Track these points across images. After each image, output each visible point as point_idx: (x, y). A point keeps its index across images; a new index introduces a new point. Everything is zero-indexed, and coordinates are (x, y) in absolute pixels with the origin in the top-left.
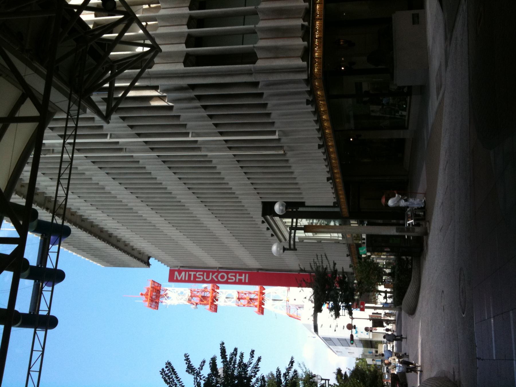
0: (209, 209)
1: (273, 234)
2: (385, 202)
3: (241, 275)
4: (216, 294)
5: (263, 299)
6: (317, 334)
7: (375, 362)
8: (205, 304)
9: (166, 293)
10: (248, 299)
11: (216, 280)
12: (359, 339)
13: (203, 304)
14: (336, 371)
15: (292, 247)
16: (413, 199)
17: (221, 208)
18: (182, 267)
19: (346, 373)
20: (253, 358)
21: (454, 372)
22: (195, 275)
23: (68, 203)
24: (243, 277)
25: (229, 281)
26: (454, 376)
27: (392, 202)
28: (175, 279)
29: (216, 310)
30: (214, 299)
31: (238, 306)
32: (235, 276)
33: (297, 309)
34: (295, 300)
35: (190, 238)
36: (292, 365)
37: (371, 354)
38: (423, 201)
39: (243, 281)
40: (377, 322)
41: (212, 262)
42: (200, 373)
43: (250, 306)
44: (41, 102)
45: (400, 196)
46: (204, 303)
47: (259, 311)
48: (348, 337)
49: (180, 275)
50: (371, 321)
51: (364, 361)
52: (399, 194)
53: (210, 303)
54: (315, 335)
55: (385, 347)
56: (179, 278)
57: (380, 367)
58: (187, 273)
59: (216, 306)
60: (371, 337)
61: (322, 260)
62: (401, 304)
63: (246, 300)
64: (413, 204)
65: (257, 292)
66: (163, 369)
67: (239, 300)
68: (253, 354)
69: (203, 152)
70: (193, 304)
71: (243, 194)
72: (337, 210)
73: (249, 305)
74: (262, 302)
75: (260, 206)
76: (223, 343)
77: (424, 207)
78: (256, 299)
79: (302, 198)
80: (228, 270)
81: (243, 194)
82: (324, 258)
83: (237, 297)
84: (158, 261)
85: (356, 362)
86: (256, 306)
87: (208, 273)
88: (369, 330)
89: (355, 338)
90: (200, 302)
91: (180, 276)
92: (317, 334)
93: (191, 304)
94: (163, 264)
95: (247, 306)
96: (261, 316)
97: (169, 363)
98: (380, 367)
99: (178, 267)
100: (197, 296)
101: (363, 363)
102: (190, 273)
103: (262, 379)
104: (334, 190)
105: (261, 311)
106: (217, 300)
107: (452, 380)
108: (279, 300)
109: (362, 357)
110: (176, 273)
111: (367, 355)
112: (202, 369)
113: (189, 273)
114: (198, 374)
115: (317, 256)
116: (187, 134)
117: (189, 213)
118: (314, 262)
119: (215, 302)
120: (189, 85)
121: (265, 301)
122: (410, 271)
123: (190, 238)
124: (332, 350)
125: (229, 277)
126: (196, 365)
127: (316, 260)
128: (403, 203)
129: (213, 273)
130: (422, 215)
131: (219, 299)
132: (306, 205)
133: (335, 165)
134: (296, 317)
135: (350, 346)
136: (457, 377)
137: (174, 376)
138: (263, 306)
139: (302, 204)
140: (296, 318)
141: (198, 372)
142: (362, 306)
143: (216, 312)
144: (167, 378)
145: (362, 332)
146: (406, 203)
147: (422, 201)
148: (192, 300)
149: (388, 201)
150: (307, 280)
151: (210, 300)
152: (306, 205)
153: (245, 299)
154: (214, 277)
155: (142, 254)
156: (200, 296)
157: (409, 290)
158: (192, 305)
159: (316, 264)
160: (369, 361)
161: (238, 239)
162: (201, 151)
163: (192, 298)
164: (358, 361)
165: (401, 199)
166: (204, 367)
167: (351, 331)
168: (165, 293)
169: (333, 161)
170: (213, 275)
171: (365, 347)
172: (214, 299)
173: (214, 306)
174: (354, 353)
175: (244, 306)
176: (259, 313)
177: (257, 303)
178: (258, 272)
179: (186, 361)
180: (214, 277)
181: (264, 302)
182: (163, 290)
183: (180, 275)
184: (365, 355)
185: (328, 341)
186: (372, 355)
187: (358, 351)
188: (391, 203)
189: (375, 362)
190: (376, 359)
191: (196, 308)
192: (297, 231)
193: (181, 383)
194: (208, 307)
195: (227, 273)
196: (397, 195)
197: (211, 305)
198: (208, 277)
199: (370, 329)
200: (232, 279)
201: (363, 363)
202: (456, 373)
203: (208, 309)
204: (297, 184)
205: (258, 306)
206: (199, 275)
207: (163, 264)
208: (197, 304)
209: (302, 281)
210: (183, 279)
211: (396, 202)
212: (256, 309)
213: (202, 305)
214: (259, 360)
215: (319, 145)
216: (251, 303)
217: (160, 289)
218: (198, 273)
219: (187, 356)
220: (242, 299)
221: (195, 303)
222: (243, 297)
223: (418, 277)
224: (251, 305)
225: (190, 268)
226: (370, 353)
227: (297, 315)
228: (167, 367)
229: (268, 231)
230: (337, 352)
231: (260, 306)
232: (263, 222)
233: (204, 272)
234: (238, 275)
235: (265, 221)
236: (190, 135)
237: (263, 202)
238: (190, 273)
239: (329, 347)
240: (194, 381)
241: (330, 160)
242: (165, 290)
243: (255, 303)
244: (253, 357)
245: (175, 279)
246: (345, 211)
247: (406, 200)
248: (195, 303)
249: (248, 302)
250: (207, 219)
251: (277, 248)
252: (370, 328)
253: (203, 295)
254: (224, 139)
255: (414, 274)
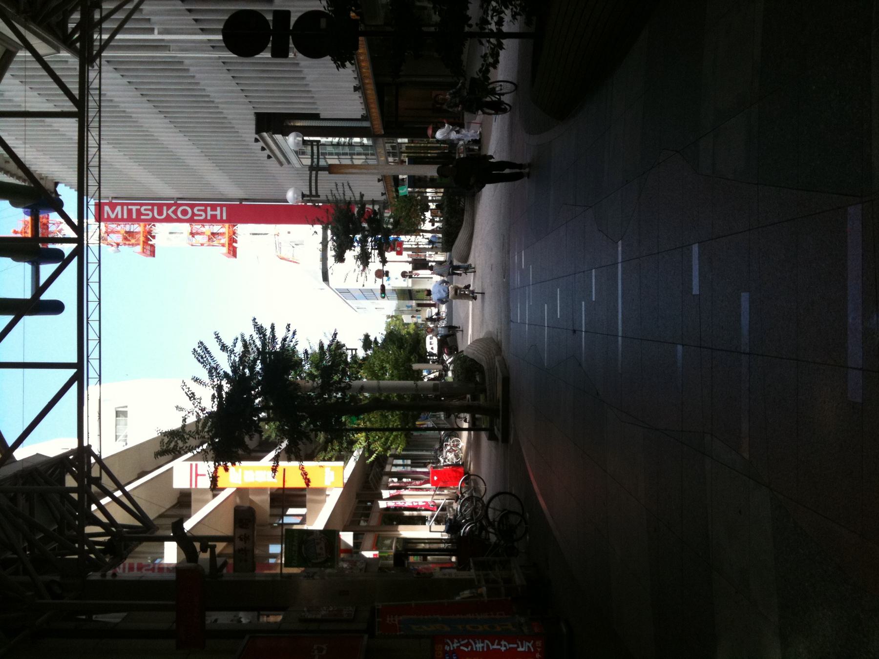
0: (136, 89)
1: (270, 154)
2: (432, 134)
3: (214, 207)
4: (151, 227)
5: (234, 233)
6: (328, 285)
7: (415, 320)
8: (133, 245)
9: (59, 228)
10: (209, 234)
11: (174, 216)
12: (391, 288)
13: (129, 245)
14: (362, 337)
15: (314, 193)
16: (467, 130)
17: (161, 93)
18: (116, 198)
19: (376, 338)
20: (289, 332)
21: (497, 332)
22: (138, 211)
23: (102, 194)
24: (218, 212)
25: (196, 218)
26: (497, 336)
27: (441, 135)
28: (106, 216)
29: (153, 254)
30: (149, 237)
31: (192, 245)
32: (205, 211)
33: (293, 247)
34: (289, 233)
35: (143, 165)
36: (335, 337)
37: (410, 309)
38: (479, 132)
39: (219, 218)
40: (420, 264)
41: (164, 189)
42: (233, 350)
43: (213, 246)
44: (77, 97)
45: (451, 127)
46: (130, 243)
47: (229, 253)
48: (378, 286)
49: (113, 212)
50: (411, 264)
51: (398, 319)
52: (450, 124)
53: (141, 243)
54: (324, 285)
55: (429, 312)
56: (113, 216)
57: (422, 326)
58: (125, 207)
59: (153, 246)
60: (410, 285)
61: (344, 191)
62: (451, 250)
63: (205, 236)
64: (466, 136)
65: (229, 225)
66: (194, 349)
67: (193, 236)
68: (289, 327)
69: (173, 52)
70: (112, 246)
71: (226, 103)
72: (366, 124)
73: (212, 244)
74: (234, 238)
75: (253, 117)
76: (255, 319)
77: (480, 139)
78: (223, 234)
79: (316, 109)
80: (193, 201)
81: (226, 103)
82: (347, 188)
83: (190, 231)
84: (66, 186)
85: (386, 321)
86: (223, 245)
87: (160, 207)
88: (407, 276)
89: (387, 287)
90: (124, 242)
91: (113, 212)
92: (328, 285)
93: (107, 245)
94: (69, 187)
95: (208, 245)
96: (233, 259)
97: (201, 343)
98: (422, 326)
99: (108, 198)
100: (118, 232)
101: (398, 322)
102: (130, 207)
103: (305, 353)
104: (362, 99)
105: (232, 252)
106: (154, 237)
107: (496, 340)
108: (261, 234)
109: (396, 313)
110: (107, 208)
111: (403, 311)
112: (235, 346)
113: (127, 207)
114: (232, 351)
115: (337, 185)
116: (151, 31)
117: (138, 127)
118: (332, 193)
119: (151, 241)
120: (208, 40)
121: (238, 236)
122: (463, 210)
123: (143, 165)
124: (351, 307)
125: (196, 212)
126: (229, 343)
127: (335, 192)
128: (454, 136)
129: (169, 206)
130: (476, 149)
131: (156, 235)
132: (321, 117)
133: (372, 101)
134: (291, 259)
135: (378, 300)
136: (499, 338)
137: (207, 355)
138: (234, 244)
139: (316, 117)
140: (291, 261)
141: (232, 350)
142: (398, 249)
143: (154, 256)
144: (200, 358)
145: (397, 279)
146: (458, 135)
147: (477, 132)
148: (109, 239)
149: (435, 133)
150: (323, 218)
151: (142, 239)
152: (321, 117)
153: (202, 233)
154: (170, 212)
155: (45, 178)
156: (123, 232)
157: (460, 235)
158: (110, 246)
159: (335, 195)
160: (407, 319)
161: (170, 117)
162: (169, 51)
163: (108, 235)
164: (390, 320)
165: (452, 130)
166: (237, 345)
167: (381, 280)
168: (58, 229)
169: (364, 70)
170: (168, 210)
171: (400, 300)
172: (149, 237)
173: (148, 248)
174: (383, 308)
175: (202, 245)
176: (229, 255)
177: (225, 240)
178: (241, 203)
179: (216, 339)
180: (170, 212)
181: (237, 237)
182: (54, 224)
183: (113, 212)
184: (400, 311)
185: (345, 293)
186: (412, 310)
187: (390, 306)
188: (439, 135)
189: (415, 320)
190: (418, 315)
191: (118, 252)
192: (319, 172)
193: (215, 362)
194: (139, 248)
195: (192, 206)
196: (446, 125)
197: (144, 245)
198: (160, 213)
199: (408, 274)
200: (201, 215)
201: (398, 322)
202: (499, 334)
203: (139, 253)
204: (309, 91)
205: (227, 245)
206: (146, 210)
207: (69, 187)
208: (118, 245)
209: (314, 220)
210: (120, 216)
211: (446, 134)
212: (225, 250)
213: (127, 246)
214: (294, 333)
215: (382, 193)
216: (214, 239)
217: (48, 221)
218: (144, 208)
219: (218, 334)
220: (198, 233)
221: (114, 244)
222: (199, 231)
223: (471, 221)
224: (215, 243)
225: (128, 200)
226: (408, 307)
227: (293, 256)
228: (199, 347)
229: (263, 152)
230: (358, 308)
231: (230, 245)
232: (256, 140)
233: (153, 205)
234: (209, 209)
235: (272, 156)
236: (156, 31)
237: (255, 113)
238: (130, 207)
239: (345, 301)
240: (228, 359)
241: (360, 69)
242: (57, 223)
243: (220, 239)
244: (289, 331)
245: (106, 216)
246: (379, 128)
247: (458, 132)
248: (114, 244)
249: (209, 239)
250: (147, 115)
251: (294, 193)
252: (410, 272)
253: (128, 230)
254: (208, 38)
255: (466, 217)
